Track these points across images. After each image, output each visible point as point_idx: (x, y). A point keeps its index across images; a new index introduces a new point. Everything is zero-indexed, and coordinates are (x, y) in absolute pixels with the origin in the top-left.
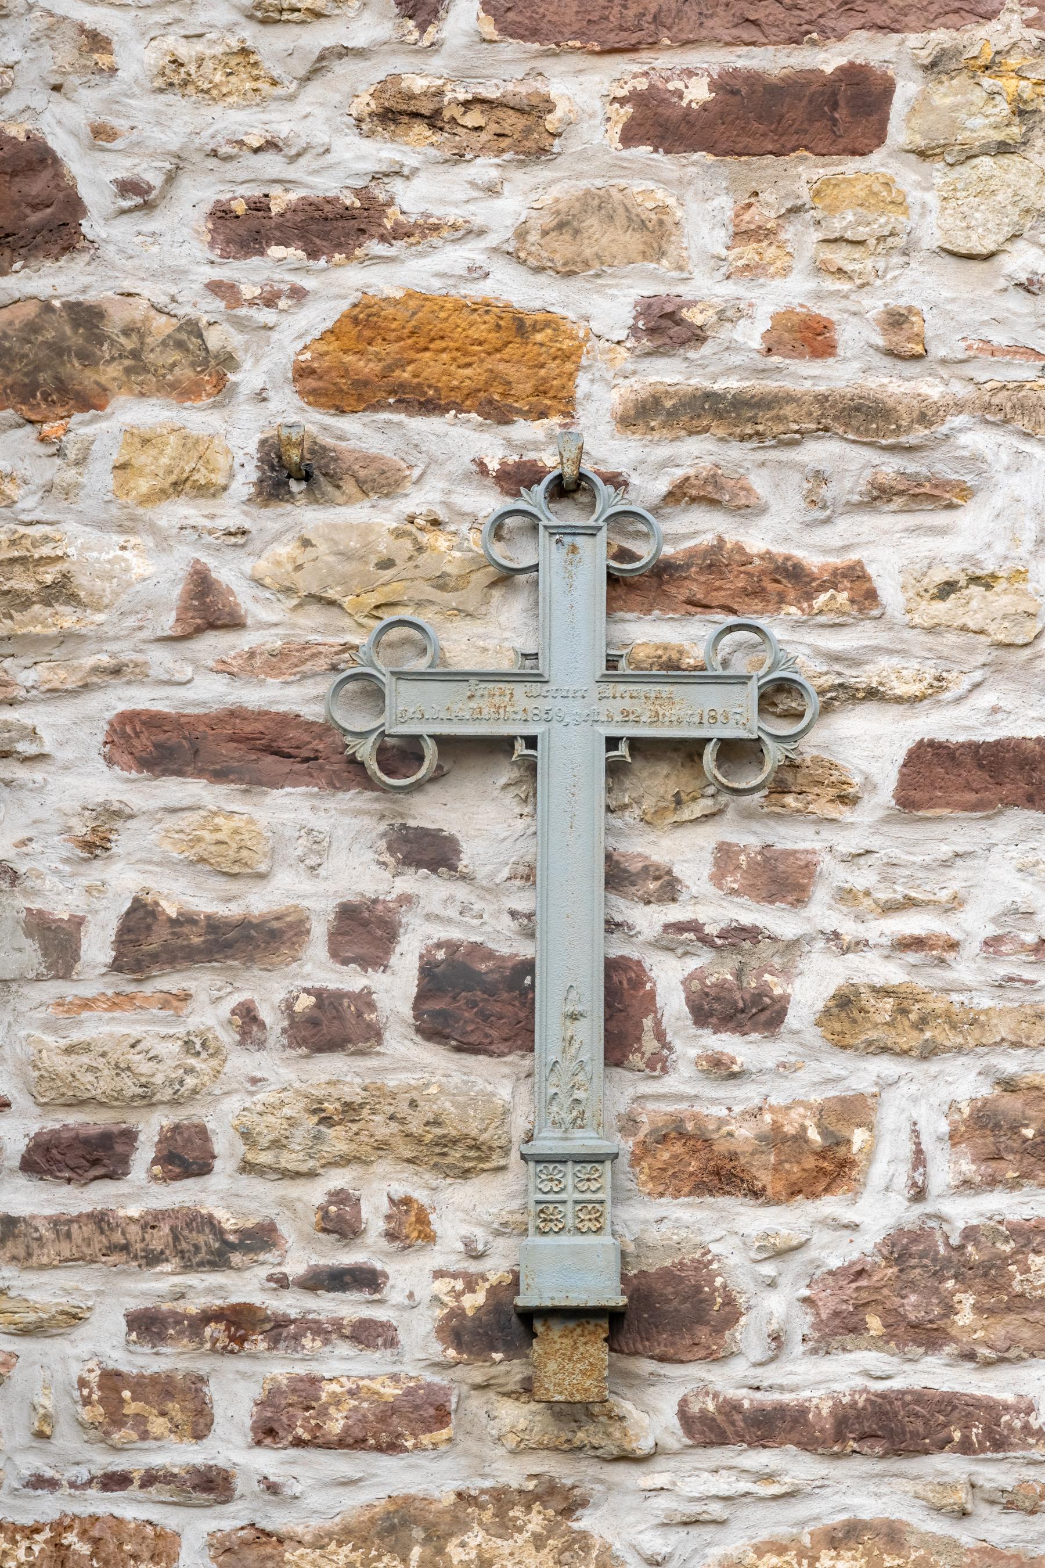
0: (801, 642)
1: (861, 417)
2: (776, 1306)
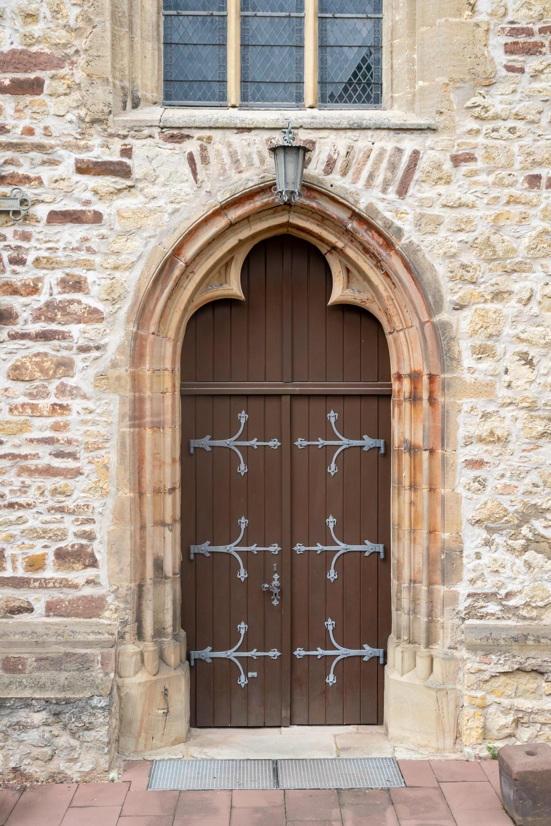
0: (29, 192)
1: (40, 147)
2: (25, 315)
